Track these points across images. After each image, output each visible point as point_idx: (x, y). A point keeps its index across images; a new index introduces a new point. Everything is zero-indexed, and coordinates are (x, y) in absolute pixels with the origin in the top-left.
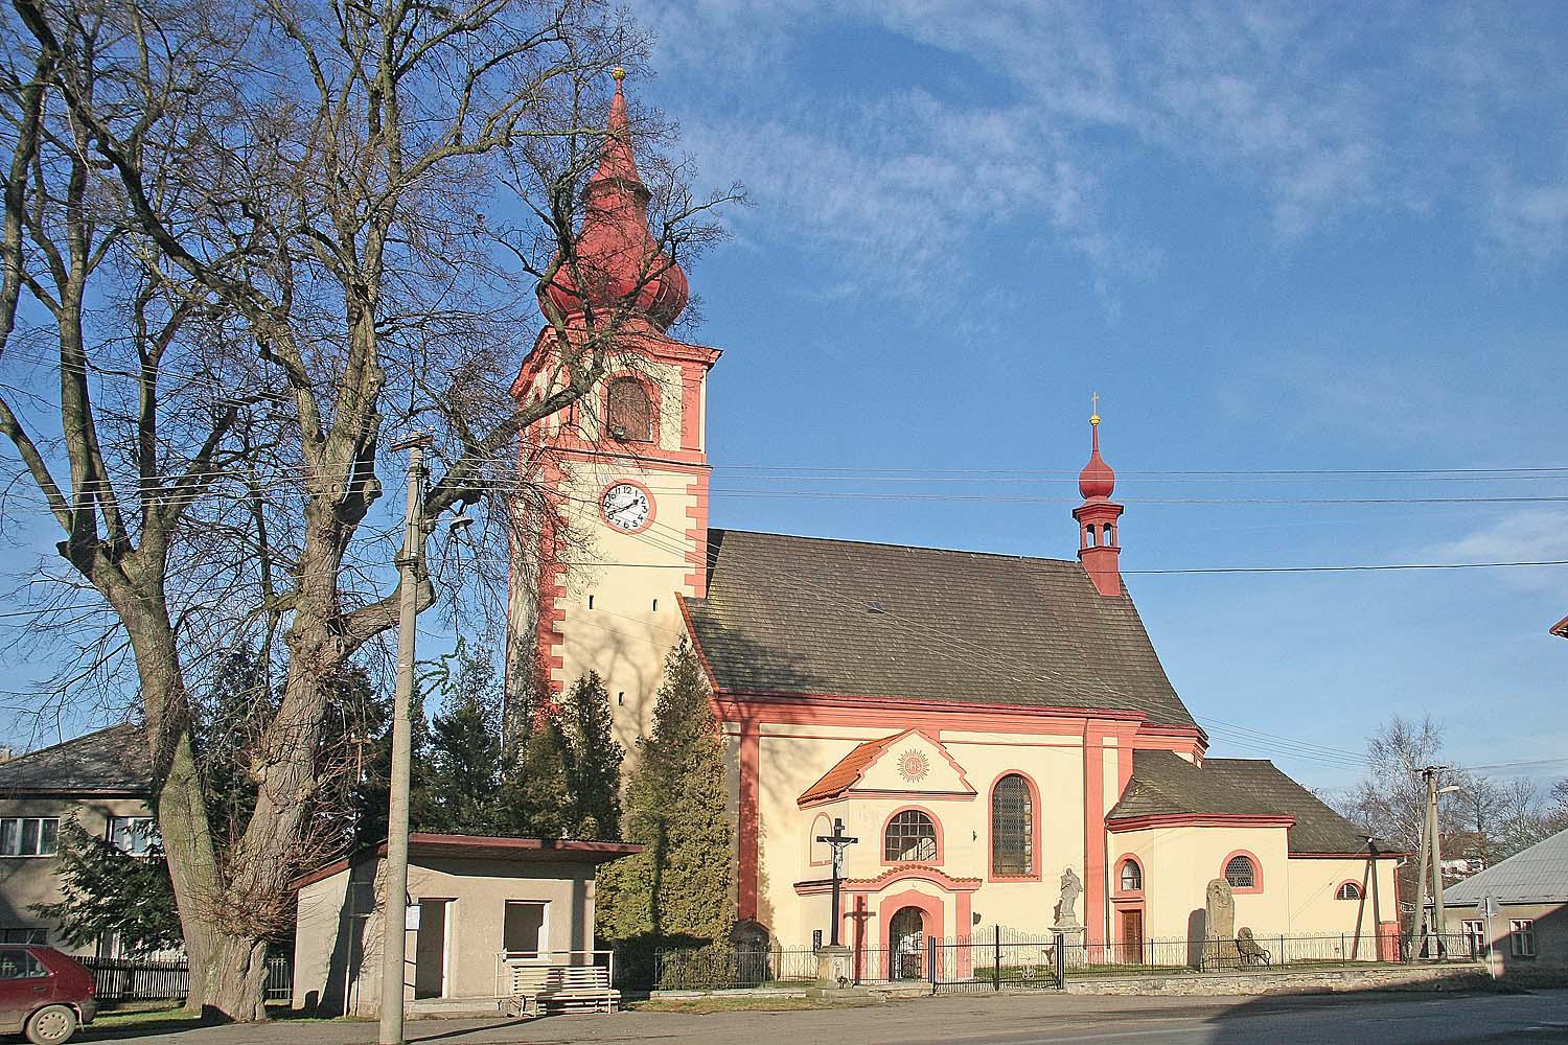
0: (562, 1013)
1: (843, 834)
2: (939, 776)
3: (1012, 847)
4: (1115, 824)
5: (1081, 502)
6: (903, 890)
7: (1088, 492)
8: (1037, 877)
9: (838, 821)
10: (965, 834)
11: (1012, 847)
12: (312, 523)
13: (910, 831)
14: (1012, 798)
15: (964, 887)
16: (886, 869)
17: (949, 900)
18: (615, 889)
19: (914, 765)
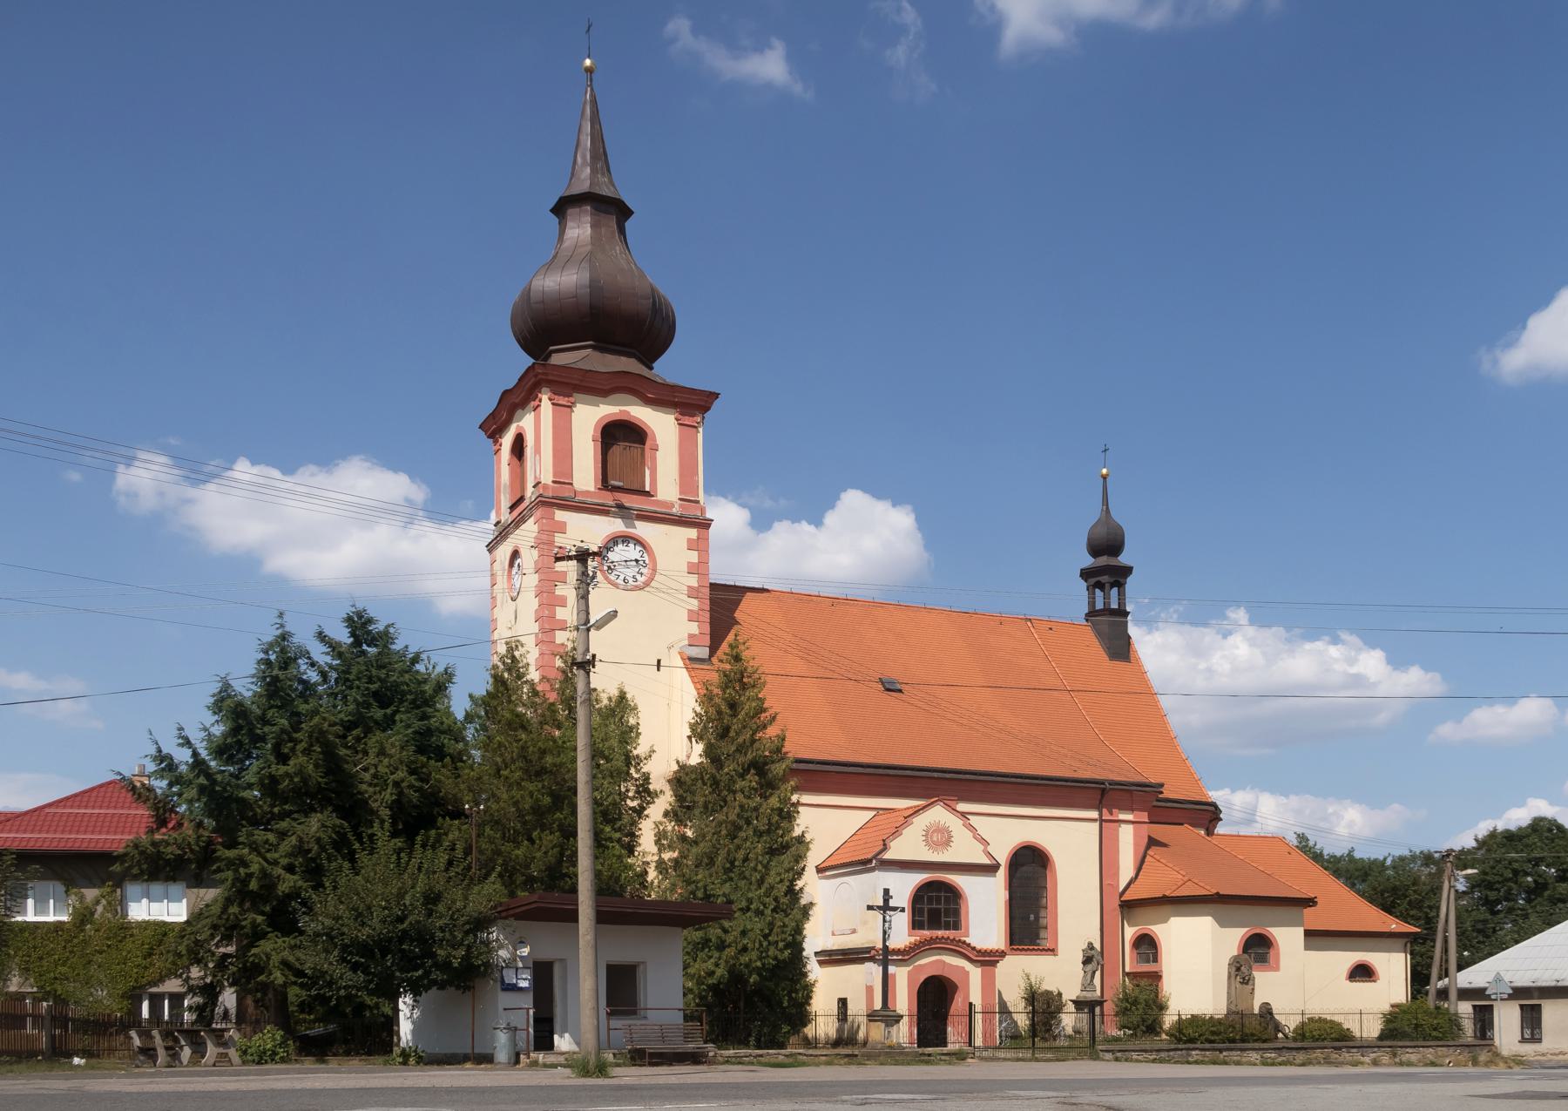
0: (327, 499)
1: (892, 903)
2: (964, 850)
3: (1028, 925)
4: (1130, 907)
5: (1088, 561)
6: (929, 963)
7: (1095, 550)
8: (1052, 951)
9: (886, 891)
10: (985, 911)
11: (1028, 925)
12: (534, 705)
13: (937, 906)
14: (1029, 869)
15: (988, 960)
16: (912, 939)
17: (975, 973)
18: (748, 823)
19: (940, 837)
